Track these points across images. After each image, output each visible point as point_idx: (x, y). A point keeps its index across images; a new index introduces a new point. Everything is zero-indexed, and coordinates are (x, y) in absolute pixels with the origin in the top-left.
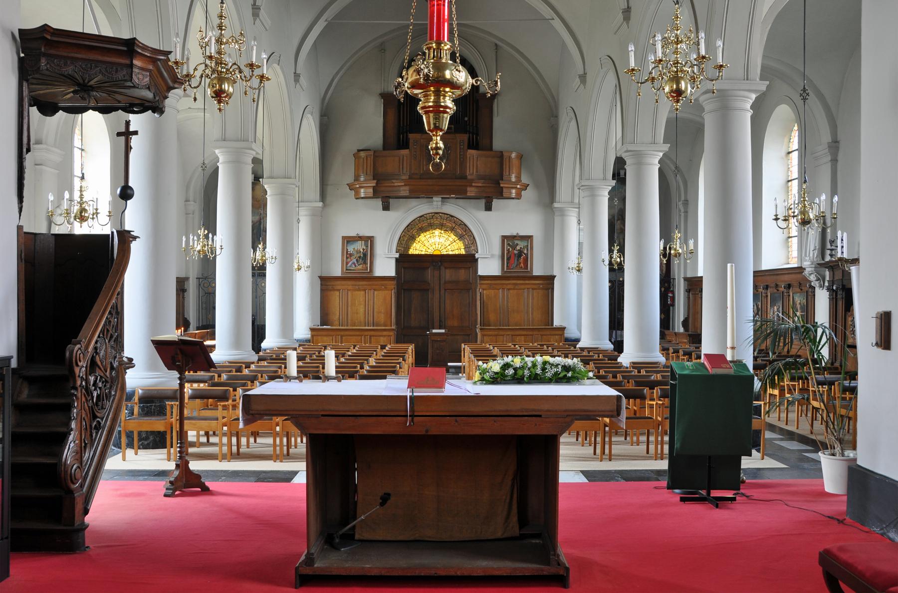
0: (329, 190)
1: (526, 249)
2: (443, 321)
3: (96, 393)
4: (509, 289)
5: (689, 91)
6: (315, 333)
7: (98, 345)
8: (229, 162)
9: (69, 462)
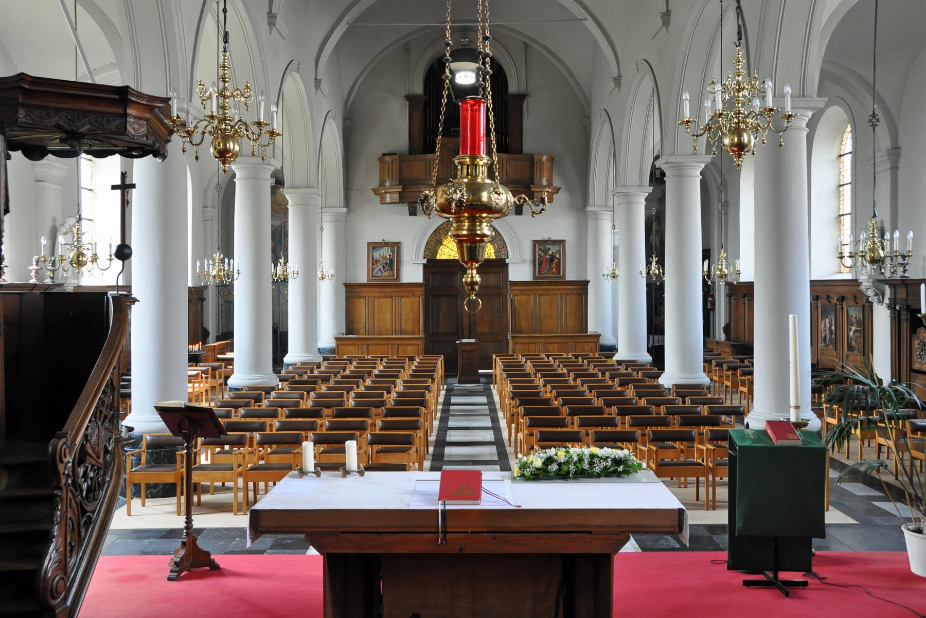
0: (354, 195)
1: (558, 254)
2: (473, 327)
3: (86, 484)
4: (541, 295)
5: (752, 144)
6: (340, 342)
7: (90, 430)
8: (246, 178)
9: (49, 575)
